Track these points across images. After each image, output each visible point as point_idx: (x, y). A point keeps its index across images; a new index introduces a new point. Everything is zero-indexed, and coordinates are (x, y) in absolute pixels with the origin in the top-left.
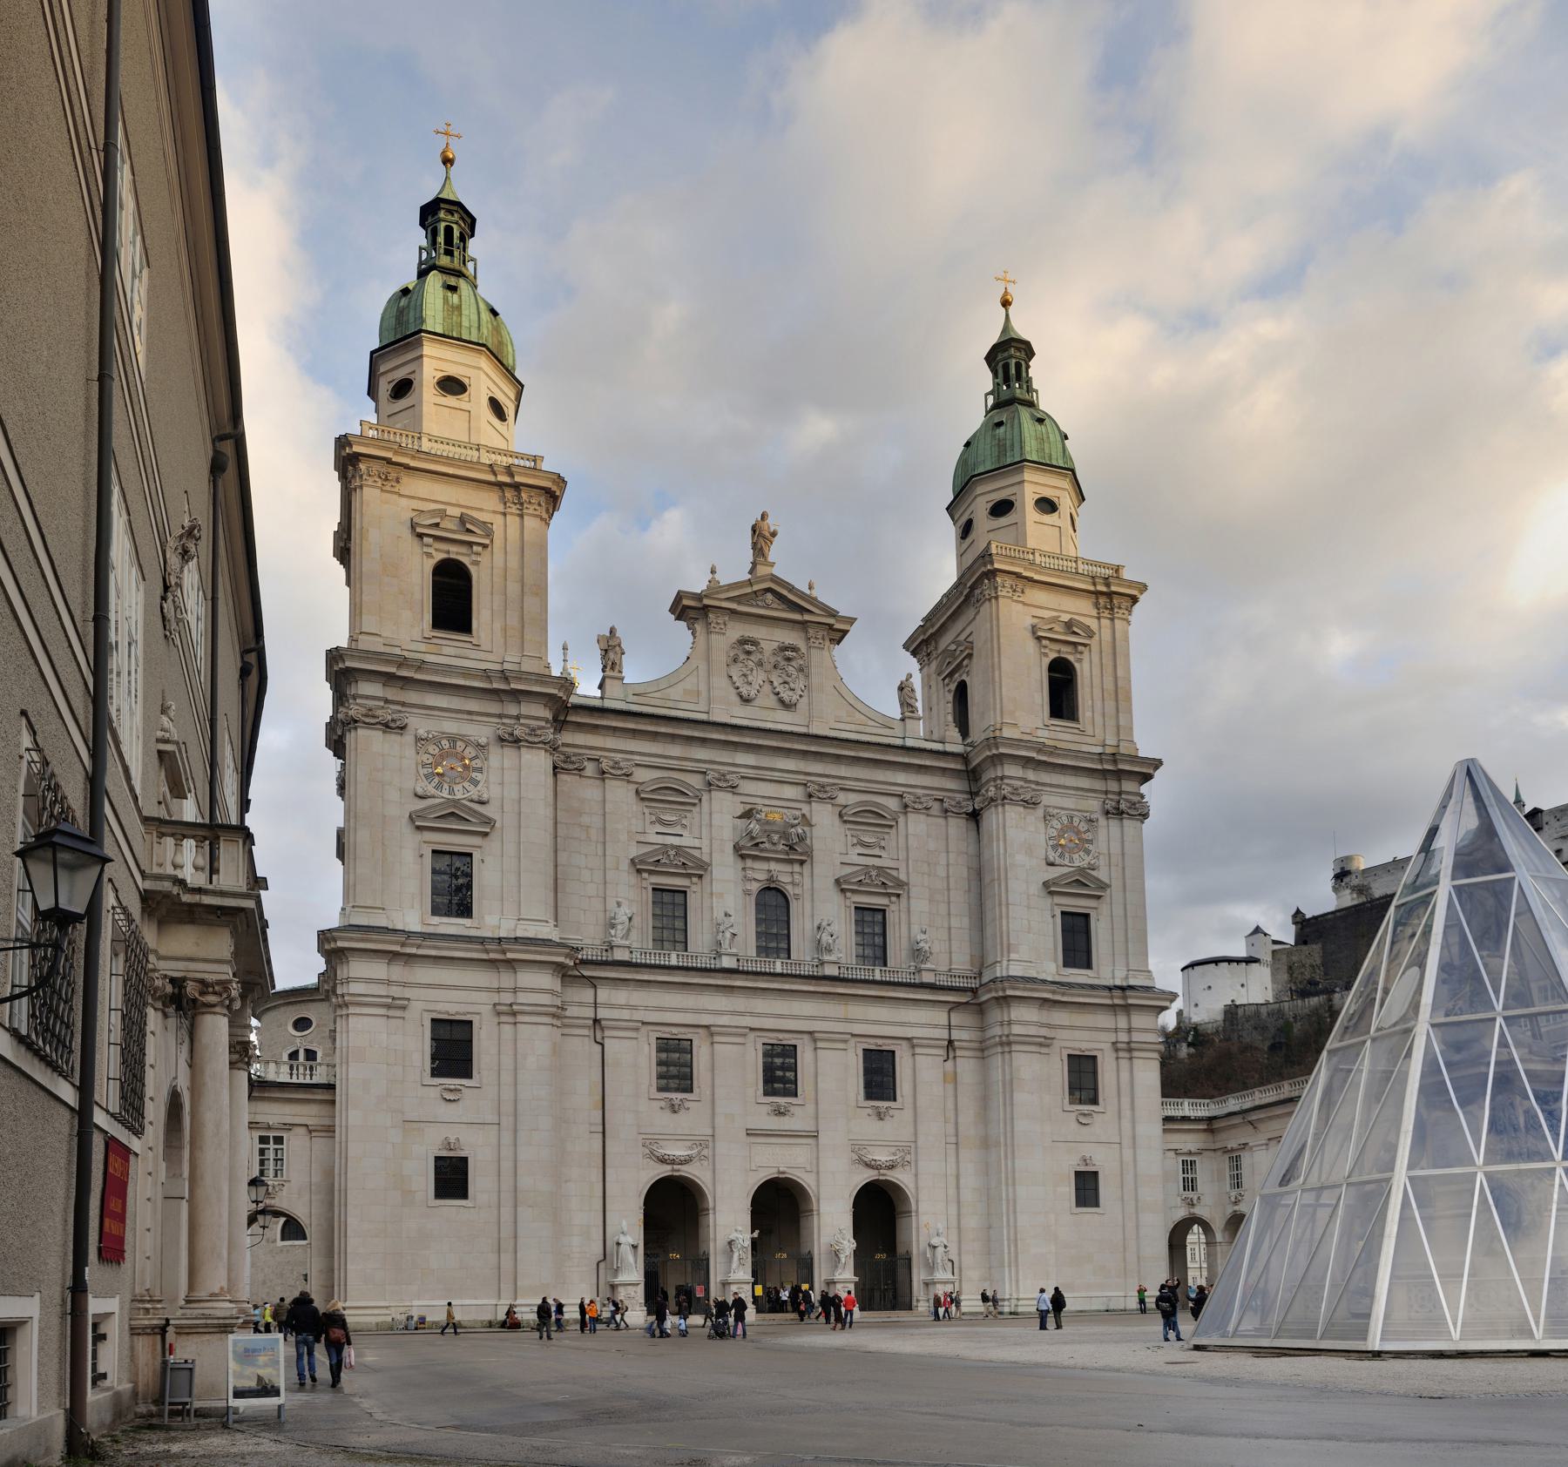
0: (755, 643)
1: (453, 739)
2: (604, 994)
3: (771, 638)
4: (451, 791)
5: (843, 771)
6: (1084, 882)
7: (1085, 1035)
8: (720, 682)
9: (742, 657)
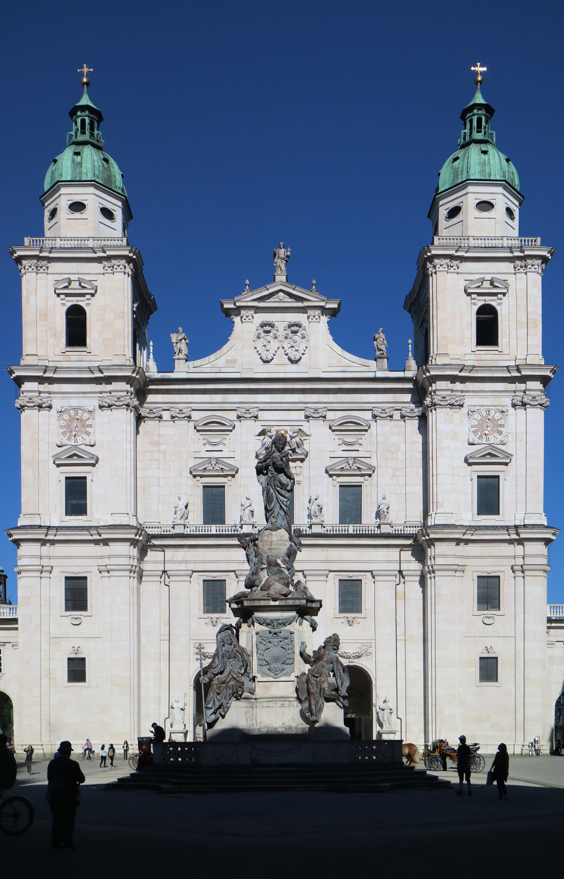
0: (272, 325)
1: (76, 409)
2: (169, 553)
4: (76, 441)
6: (493, 455)
7: (491, 561)
9: (263, 334)
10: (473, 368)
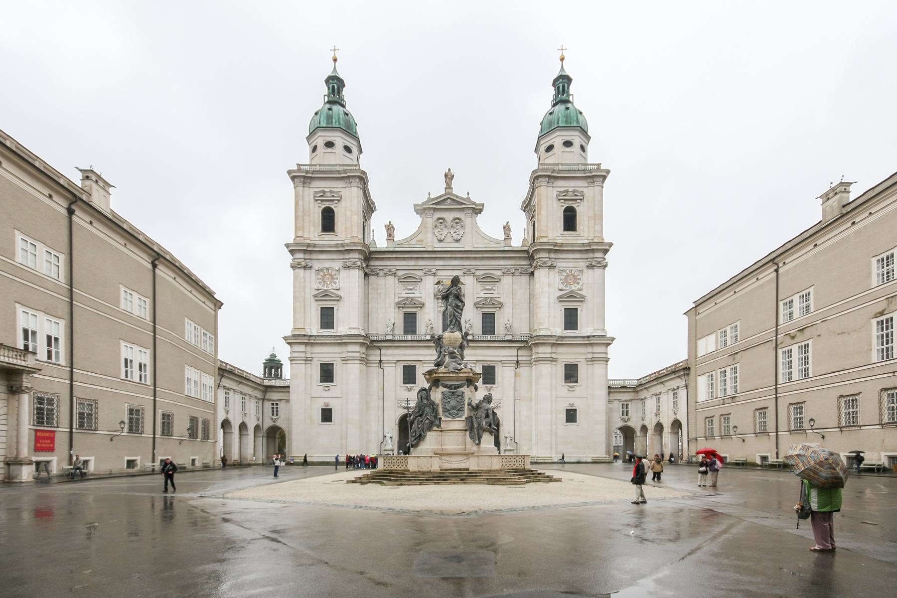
0: (443, 219)
1: (328, 269)
2: (383, 351)
3: (449, 216)
5: (478, 262)
7: (573, 356)
8: (430, 235)
10: (562, 245)
